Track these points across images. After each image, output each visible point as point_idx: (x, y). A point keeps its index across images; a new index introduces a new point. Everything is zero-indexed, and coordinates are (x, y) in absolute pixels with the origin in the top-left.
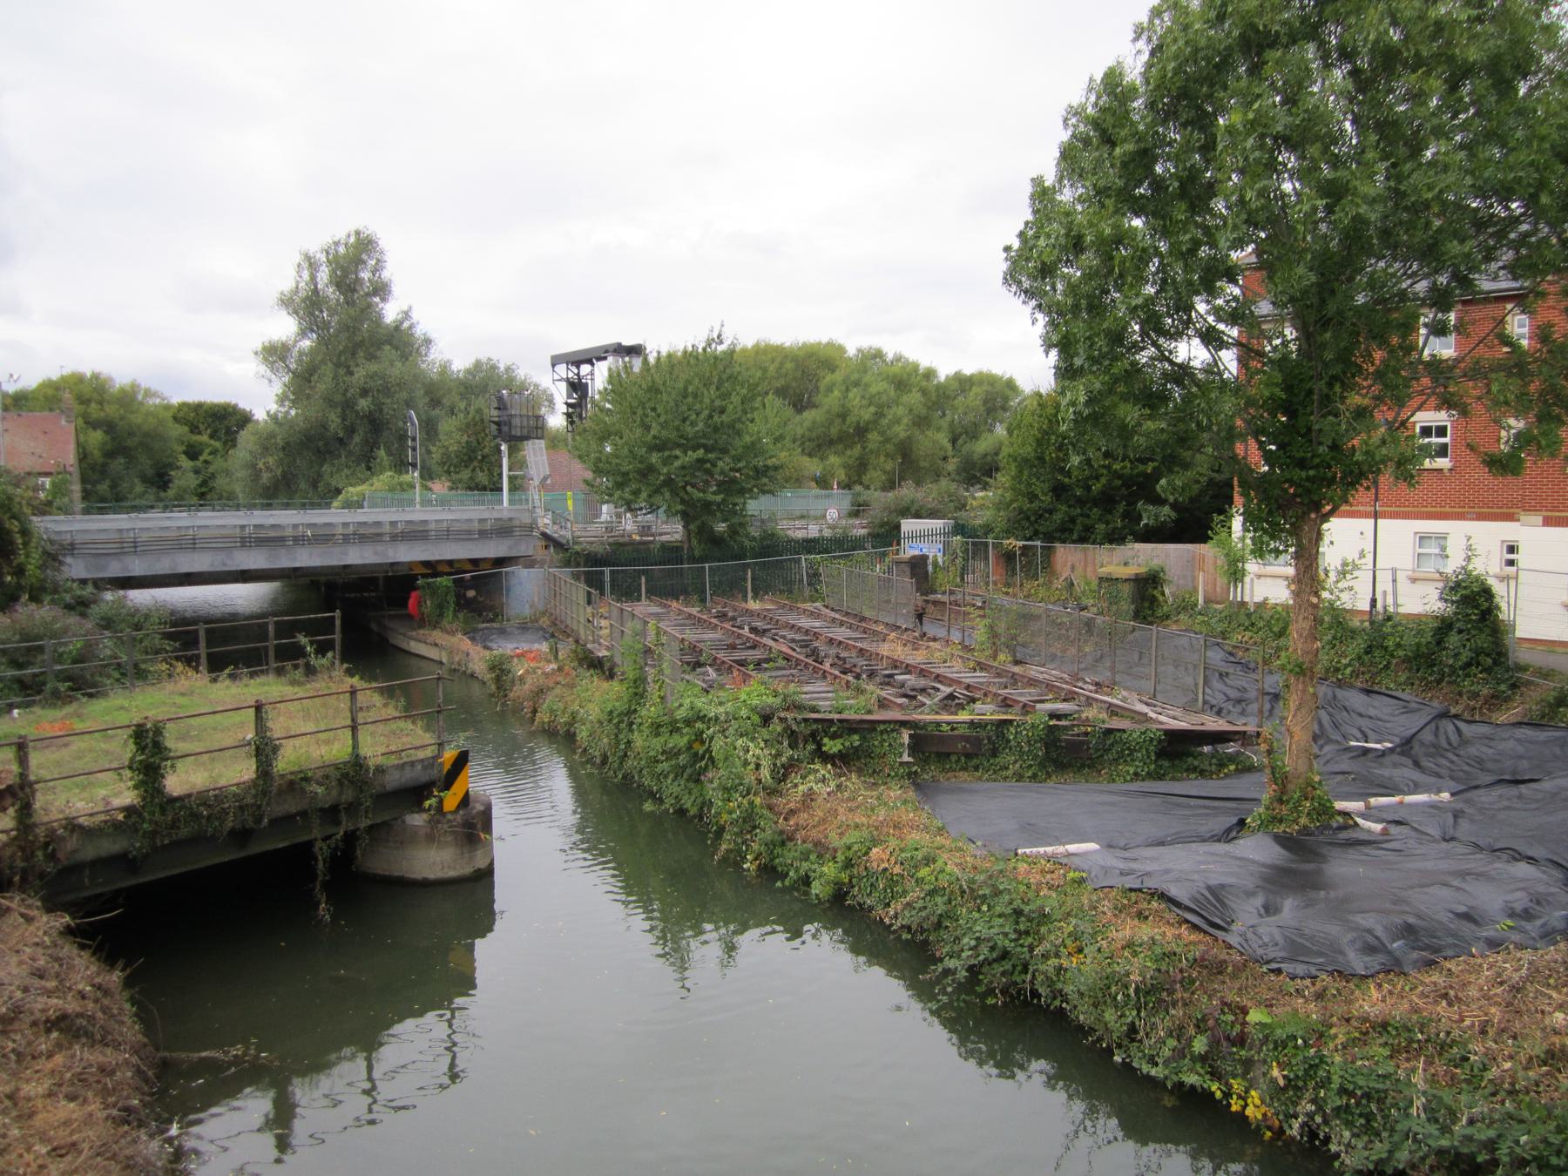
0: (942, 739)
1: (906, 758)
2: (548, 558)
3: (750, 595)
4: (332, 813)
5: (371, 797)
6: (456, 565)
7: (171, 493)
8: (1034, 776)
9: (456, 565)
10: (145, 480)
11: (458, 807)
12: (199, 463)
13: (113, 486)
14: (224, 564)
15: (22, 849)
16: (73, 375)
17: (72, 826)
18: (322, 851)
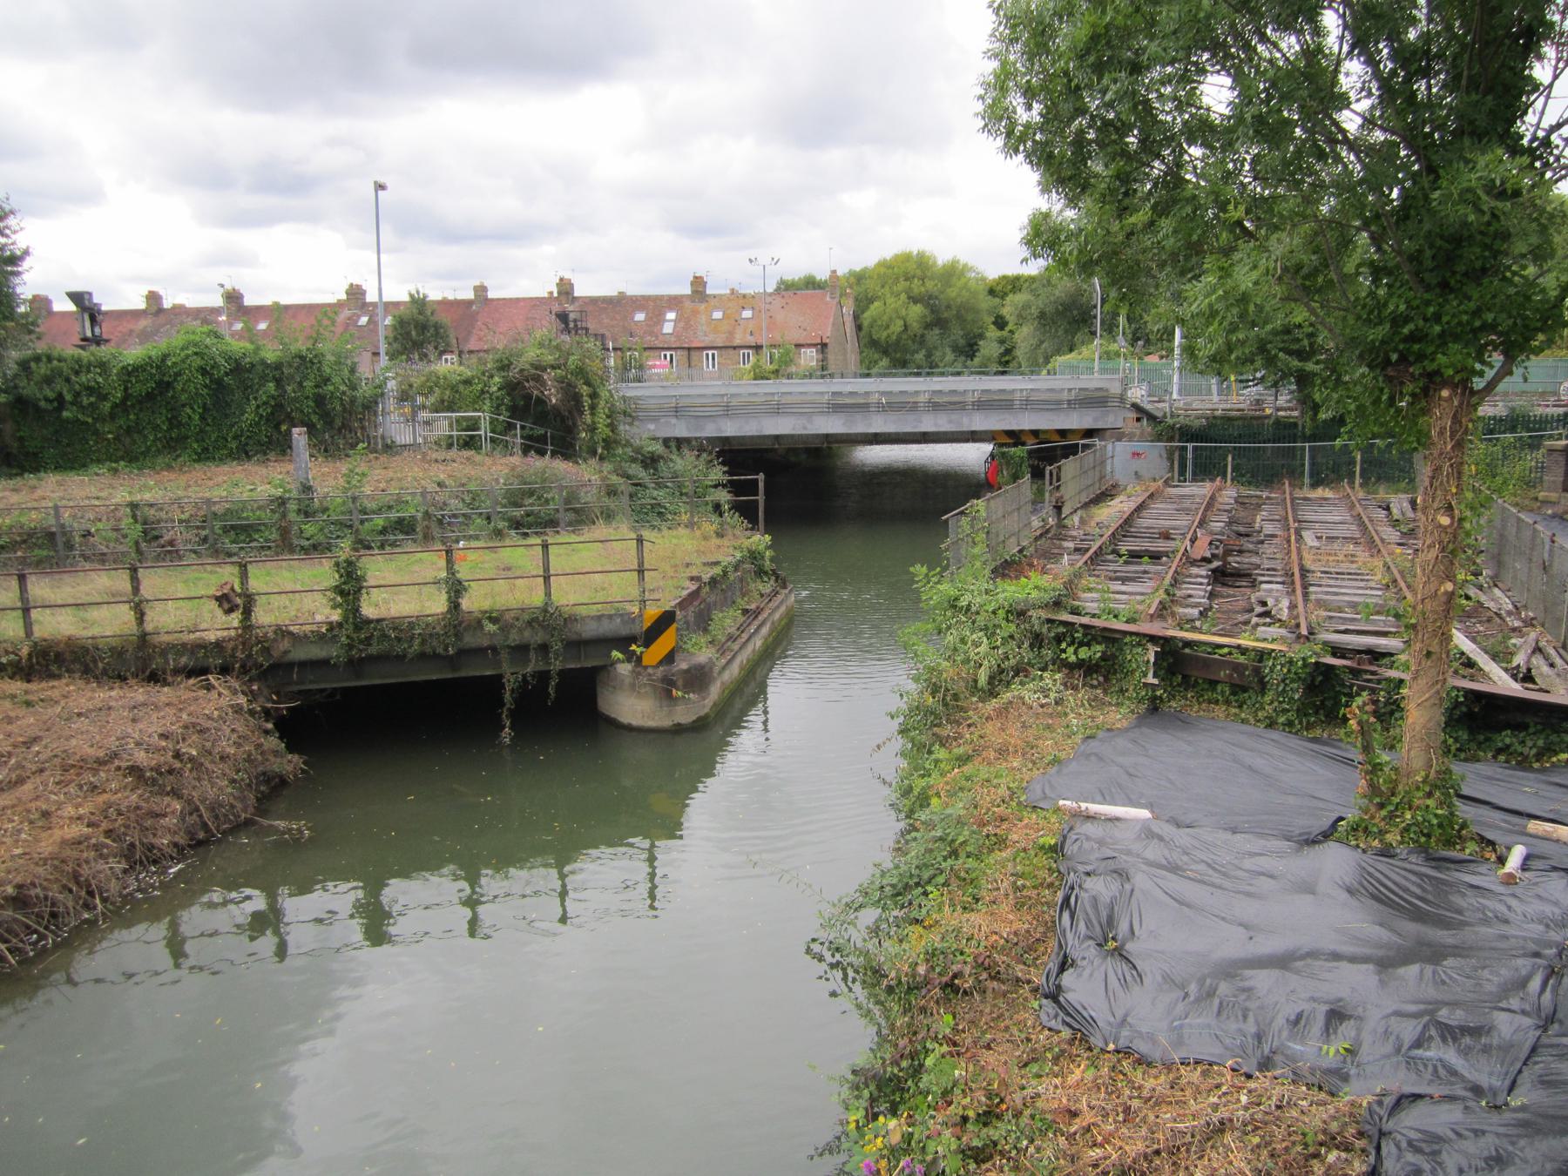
0: (1207, 664)
1: (1151, 679)
2: (1138, 432)
3: (1358, 480)
4: (521, 650)
5: (562, 641)
6: (1042, 436)
7: (976, 360)
8: (1290, 724)
9: (1042, 436)
10: (957, 349)
11: (661, 663)
12: (1005, 333)
13: (929, 355)
14: (805, 428)
15: (244, 644)
16: (907, 257)
17: (282, 632)
18: (510, 682)
